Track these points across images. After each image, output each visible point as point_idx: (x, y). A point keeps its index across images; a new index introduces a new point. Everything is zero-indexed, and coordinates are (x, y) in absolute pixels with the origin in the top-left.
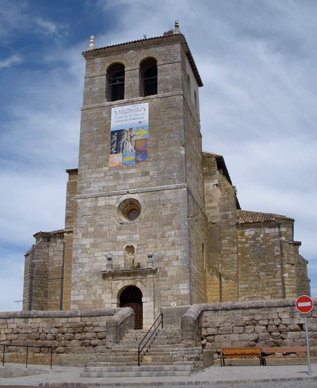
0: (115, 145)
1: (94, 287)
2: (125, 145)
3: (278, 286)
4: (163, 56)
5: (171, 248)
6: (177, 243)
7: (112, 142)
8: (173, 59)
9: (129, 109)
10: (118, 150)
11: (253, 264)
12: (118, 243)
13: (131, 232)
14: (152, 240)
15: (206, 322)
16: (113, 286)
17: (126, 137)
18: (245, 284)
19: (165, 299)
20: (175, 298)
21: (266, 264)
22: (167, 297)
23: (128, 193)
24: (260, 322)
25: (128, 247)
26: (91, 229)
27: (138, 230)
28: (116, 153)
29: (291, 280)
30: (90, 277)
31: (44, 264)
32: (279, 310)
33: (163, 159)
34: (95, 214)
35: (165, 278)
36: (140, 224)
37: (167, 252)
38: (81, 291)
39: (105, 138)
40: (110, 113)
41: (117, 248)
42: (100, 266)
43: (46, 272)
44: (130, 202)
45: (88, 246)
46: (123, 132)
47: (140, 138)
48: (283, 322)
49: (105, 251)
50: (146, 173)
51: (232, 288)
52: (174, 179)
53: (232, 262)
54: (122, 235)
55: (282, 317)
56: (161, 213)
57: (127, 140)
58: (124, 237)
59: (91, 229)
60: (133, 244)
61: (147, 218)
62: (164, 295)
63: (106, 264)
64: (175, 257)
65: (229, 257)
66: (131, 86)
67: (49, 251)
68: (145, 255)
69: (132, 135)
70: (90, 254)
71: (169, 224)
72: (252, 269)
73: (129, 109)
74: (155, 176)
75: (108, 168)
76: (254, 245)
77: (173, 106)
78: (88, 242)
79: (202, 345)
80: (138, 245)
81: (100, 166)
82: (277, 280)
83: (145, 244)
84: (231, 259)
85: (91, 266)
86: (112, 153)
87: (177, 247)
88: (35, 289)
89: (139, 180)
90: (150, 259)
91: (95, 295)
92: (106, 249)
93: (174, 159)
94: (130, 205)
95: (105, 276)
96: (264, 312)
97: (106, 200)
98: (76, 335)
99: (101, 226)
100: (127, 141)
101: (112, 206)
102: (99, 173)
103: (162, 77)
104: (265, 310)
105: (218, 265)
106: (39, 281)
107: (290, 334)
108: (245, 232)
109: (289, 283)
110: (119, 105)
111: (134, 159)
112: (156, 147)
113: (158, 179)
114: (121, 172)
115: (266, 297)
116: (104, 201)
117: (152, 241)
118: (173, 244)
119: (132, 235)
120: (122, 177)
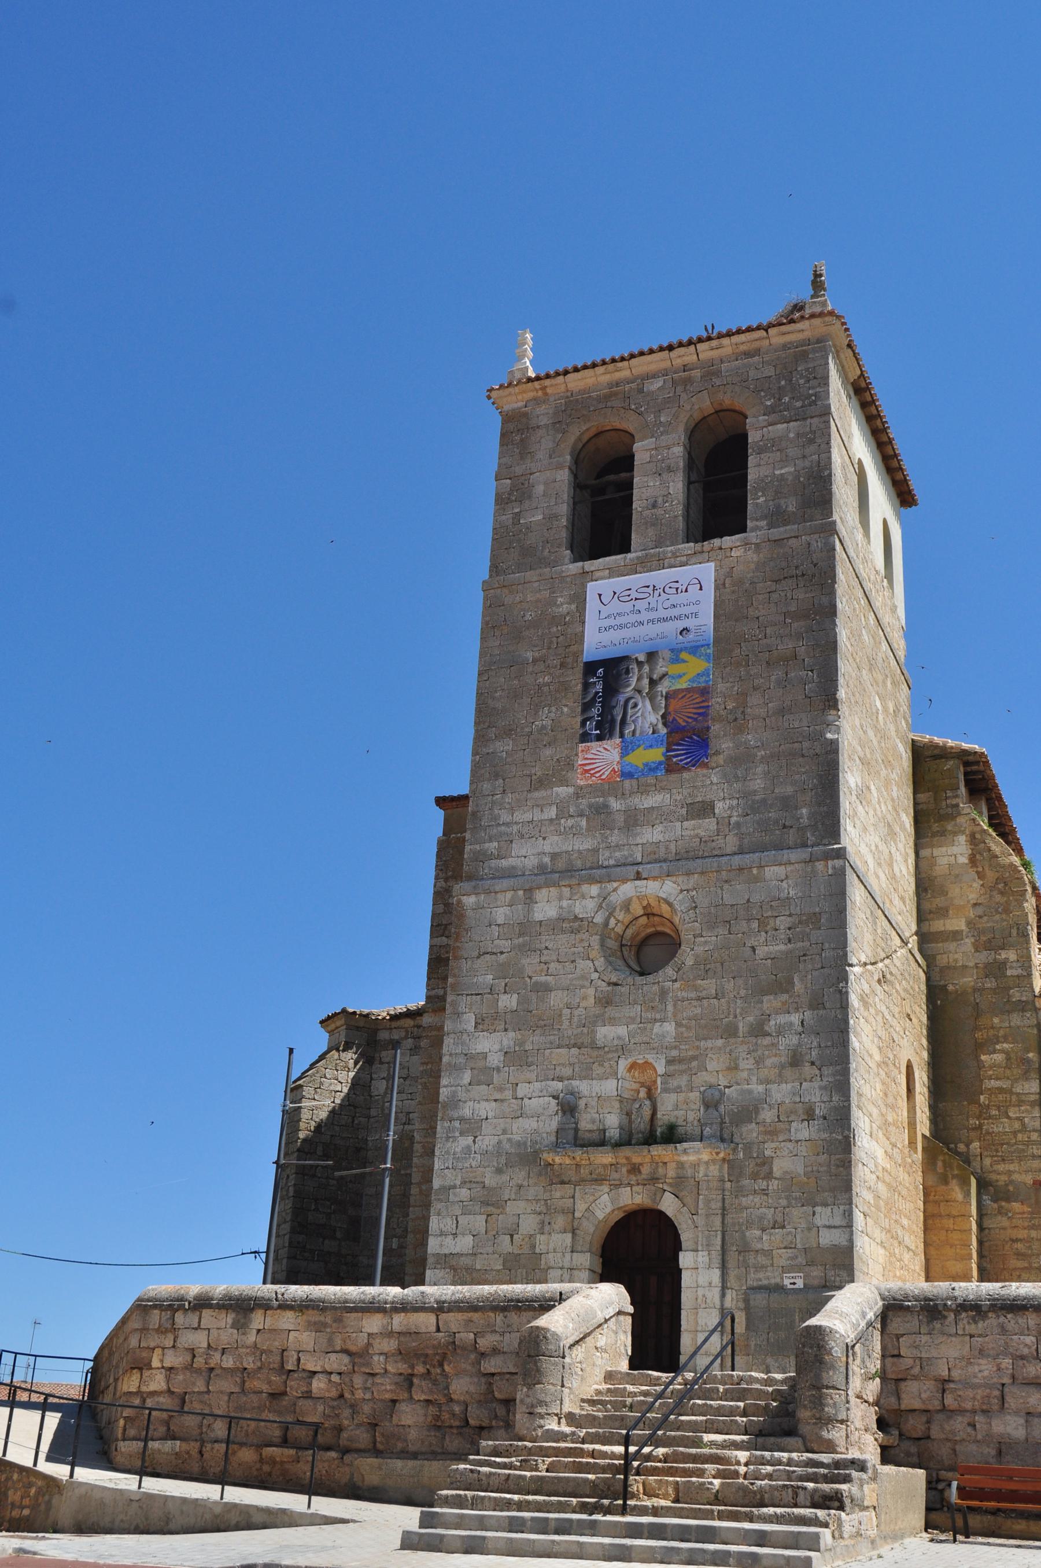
0: (595, 711)
1: (511, 1208)
2: (630, 712)
4: (766, 396)
5: (788, 1072)
7: (587, 700)
8: (802, 407)
9: (648, 587)
12: (601, 1052)
14: (720, 1042)
15: (899, 1356)
16: (581, 1207)
17: (633, 681)
19: (762, 1260)
22: (768, 1253)
26: (508, 1001)
27: (670, 1008)
28: (600, 738)
30: (499, 1171)
31: (353, 1122)
33: (762, 757)
34: (526, 949)
35: (763, 1184)
36: (677, 985)
37: (774, 1087)
39: (565, 687)
40: (580, 600)
41: (598, 1070)
43: (358, 1150)
44: (644, 908)
45: (495, 1059)
46: (623, 666)
47: (684, 686)
49: (553, 1080)
52: (802, 830)
53: (1020, 1136)
54: (613, 1021)
56: (753, 949)
57: (639, 692)
58: (622, 1031)
59: (508, 1001)
60: (650, 1058)
61: (705, 968)
62: (759, 1246)
63: (554, 1124)
65: (1009, 1117)
67: (372, 1079)
68: (695, 1096)
69: (655, 677)
73: (648, 587)
74: (733, 820)
75: (571, 790)
78: (497, 1047)
80: (670, 1062)
81: (542, 783)
83: (694, 1058)
85: (504, 1132)
86: (585, 737)
87: (808, 1070)
88: (316, 1210)
91: (512, 1236)
94: (645, 918)
100: (637, 696)
101: (582, 920)
103: (764, 471)
105: (967, 1146)
110: (614, 572)
111: (663, 759)
112: (739, 715)
113: (744, 830)
116: (555, 903)
117: (720, 1049)
119: (649, 1026)
120: (620, 819)
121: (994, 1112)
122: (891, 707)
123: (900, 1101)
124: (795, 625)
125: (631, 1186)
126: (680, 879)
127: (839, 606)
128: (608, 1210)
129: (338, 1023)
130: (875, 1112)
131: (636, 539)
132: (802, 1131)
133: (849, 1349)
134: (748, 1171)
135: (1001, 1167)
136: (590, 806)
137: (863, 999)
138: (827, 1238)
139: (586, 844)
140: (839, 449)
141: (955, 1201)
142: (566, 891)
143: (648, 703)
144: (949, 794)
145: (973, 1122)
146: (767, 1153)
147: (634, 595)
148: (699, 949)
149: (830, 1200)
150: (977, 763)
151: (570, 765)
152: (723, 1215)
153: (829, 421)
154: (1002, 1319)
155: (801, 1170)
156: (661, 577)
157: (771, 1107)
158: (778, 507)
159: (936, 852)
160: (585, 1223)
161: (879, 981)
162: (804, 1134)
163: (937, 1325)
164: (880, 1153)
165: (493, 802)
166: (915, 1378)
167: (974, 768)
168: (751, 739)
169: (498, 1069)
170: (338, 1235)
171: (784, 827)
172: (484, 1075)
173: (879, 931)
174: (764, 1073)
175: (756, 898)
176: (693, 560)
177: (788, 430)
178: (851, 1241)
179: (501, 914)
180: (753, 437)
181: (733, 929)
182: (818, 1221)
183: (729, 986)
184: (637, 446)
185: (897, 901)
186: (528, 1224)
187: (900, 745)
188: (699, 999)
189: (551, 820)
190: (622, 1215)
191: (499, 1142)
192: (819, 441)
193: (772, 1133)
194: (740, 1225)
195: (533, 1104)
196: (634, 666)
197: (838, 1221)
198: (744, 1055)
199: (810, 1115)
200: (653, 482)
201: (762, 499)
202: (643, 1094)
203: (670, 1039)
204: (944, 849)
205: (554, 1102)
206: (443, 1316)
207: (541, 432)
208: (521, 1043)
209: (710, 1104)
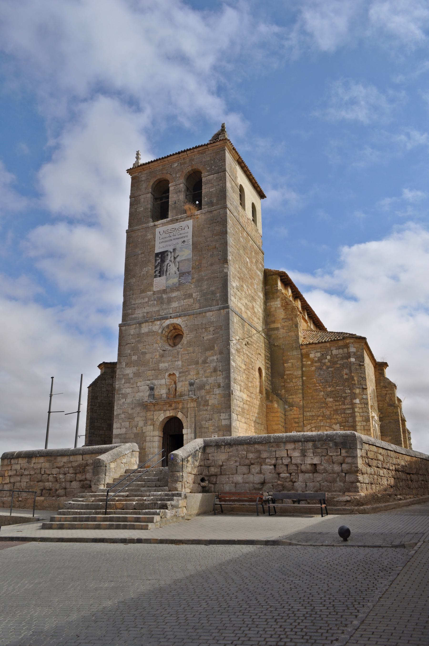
0: (158, 268)
1: (136, 419)
2: (168, 268)
3: (349, 414)
5: (213, 374)
6: (218, 369)
10: (161, 273)
11: (319, 388)
12: (161, 371)
13: (174, 359)
14: (194, 366)
15: (209, 460)
16: (155, 418)
17: (169, 258)
18: (310, 411)
19: (206, 430)
20: (217, 430)
21: (334, 389)
22: (207, 428)
23: (171, 317)
24: (267, 460)
25: (170, 375)
26: (135, 358)
27: (180, 357)
28: (160, 276)
29: (363, 406)
30: (132, 409)
32: (290, 446)
33: (206, 279)
34: (139, 342)
35: (206, 408)
36: (182, 350)
37: (209, 379)
38: (123, 424)
40: (154, 234)
41: (160, 377)
42: (143, 396)
43: (110, 404)
45: (131, 376)
48: (294, 461)
50: (190, 296)
51: (296, 416)
52: (217, 301)
54: (164, 362)
55: (292, 455)
56: (203, 337)
57: (171, 261)
58: (166, 365)
59: (135, 358)
60: (175, 372)
61: (190, 344)
62: (205, 426)
63: (148, 394)
64: (216, 384)
65: (293, 382)
66: (175, 203)
68: (187, 383)
69: (175, 256)
70: (133, 384)
71: (211, 348)
72: (318, 395)
74: (198, 298)
75: (152, 292)
76: (320, 368)
77: (217, 221)
78: (132, 372)
79: (202, 487)
80: (180, 373)
81: (143, 291)
82: (347, 406)
83: (187, 371)
84: (295, 384)
85: (134, 397)
86: (156, 276)
87: (219, 373)
88: (97, 422)
89: (182, 303)
90: (192, 387)
92: (149, 378)
93: (217, 279)
95: (145, 406)
96: (271, 449)
97: (149, 326)
98: (78, 475)
99: (144, 353)
100: (170, 262)
101: (155, 332)
102: (143, 298)
104: (272, 447)
105: (281, 391)
106: (102, 414)
107: (301, 477)
108: (310, 355)
109: (361, 411)
110: (163, 224)
112: (200, 267)
113: (201, 301)
114: (164, 296)
115: (334, 426)
116: (147, 327)
118: (215, 370)
120: (166, 301)
121: (288, 381)
122: (254, 261)
123: (255, 380)
124: (215, 237)
125: (169, 411)
126: (182, 318)
127: (229, 231)
128: (163, 418)
129: (103, 366)
130: (242, 384)
131: (170, 213)
132: (217, 391)
133: (183, 460)
134: (202, 404)
135: (290, 397)
136: (157, 297)
137: (238, 351)
138: (224, 423)
139: (156, 309)
140: (230, 181)
141: (275, 408)
142: (150, 323)
143: (173, 264)
144: (275, 286)
145: (283, 384)
146: (207, 398)
147: (169, 231)
148: (188, 339)
149: (225, 411)
150: (284, 276)
151: (152, 285)
152: (195, 418)
153: (225, 173)
154: (237, 447)
155: (217, 403)
156: (176, 225)
157: (208, 385)
158: (211, 201)
159: (271, 304)
160: (157, 422)
161: (246, 345)
162: (218, 392)
163: (219, 450)
164: (245, 396)
165: (130, 298)
166: (213, 466)
167: (284, 277)
168: (203, 273)
169: (132, 378)
170: (104, 429)
171: (212, 300)
172: (128, 381)
173: (246, 329)
174: (206, 374)
175: (204, 322)
176: (186, 219)
177: (214, 177)
178: (231, 423)
179: (132, 332)
180: (204, 179)
181: (198, 332)
182: (222, 418)
183: (197, 349)
184: (170, 185)
185: (256, 319)
186: (141, 424)
187: (258, 272)
188: (188, 353)
189: (146, 302)
190: (168, 419)
191: (133, 400)
192: (222, 179)
193: (208, 392)
194: (200, 420)
195: (142, 388)
196: (169, 253)
197: (227, 417)
198: (201, 369)
199: (219, 386)
200: (175, 196)
201: (206, 199)
202: (173, 382)
203: (180, 366)
204: (273, 303)
205: (148, 387)
206: (84, 456)
207: (143, 182)
208: (138, 370)
209: (191, 384)
